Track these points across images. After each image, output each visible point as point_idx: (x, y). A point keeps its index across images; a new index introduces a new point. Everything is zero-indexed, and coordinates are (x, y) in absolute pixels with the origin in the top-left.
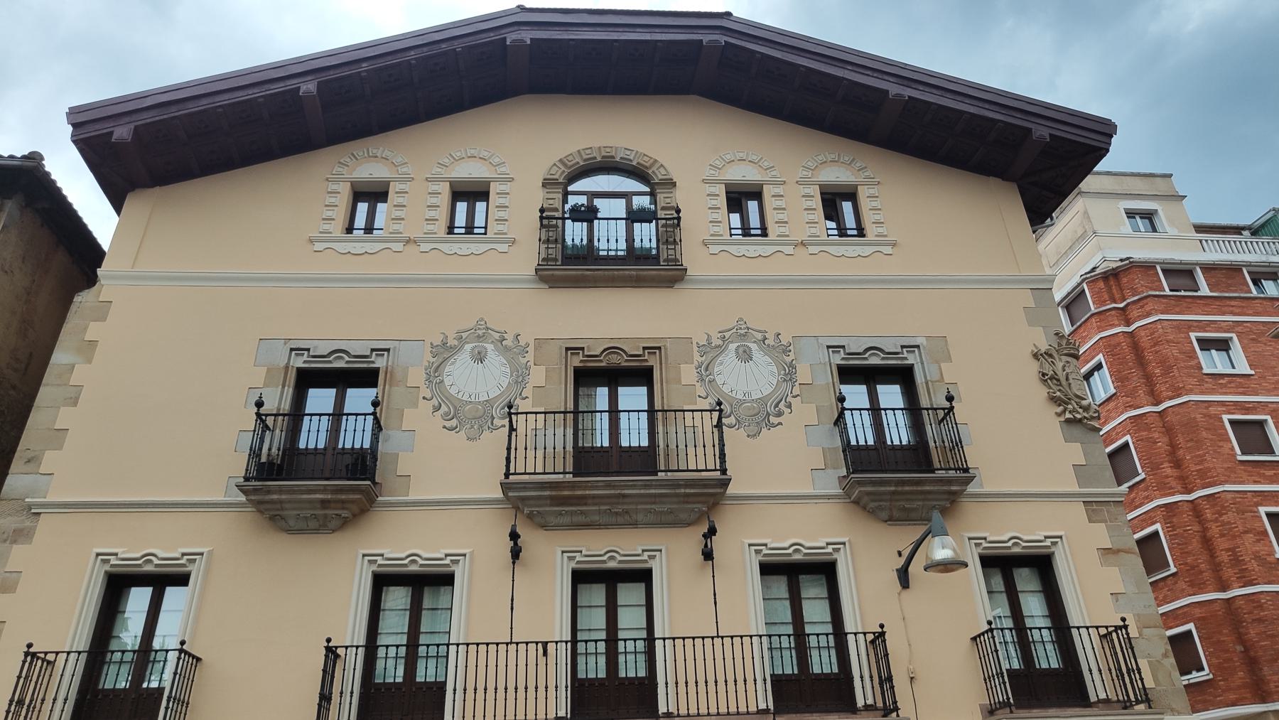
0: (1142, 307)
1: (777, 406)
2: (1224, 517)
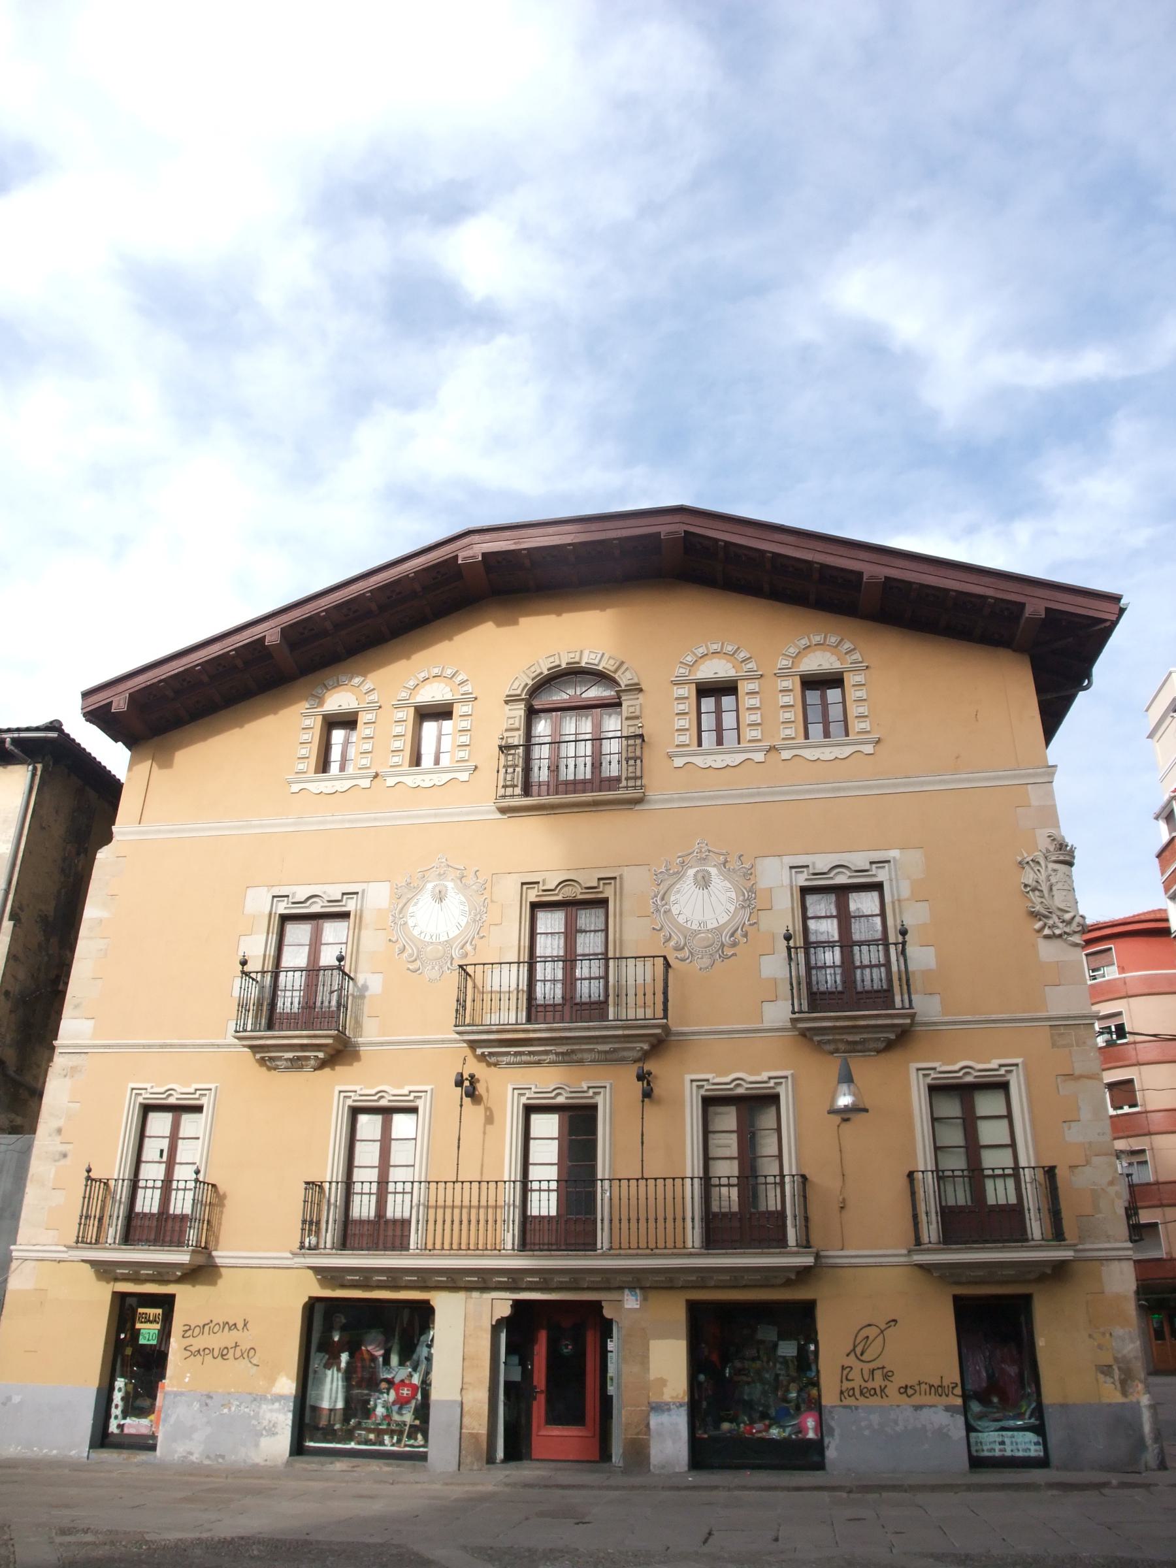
1: (732, 935)
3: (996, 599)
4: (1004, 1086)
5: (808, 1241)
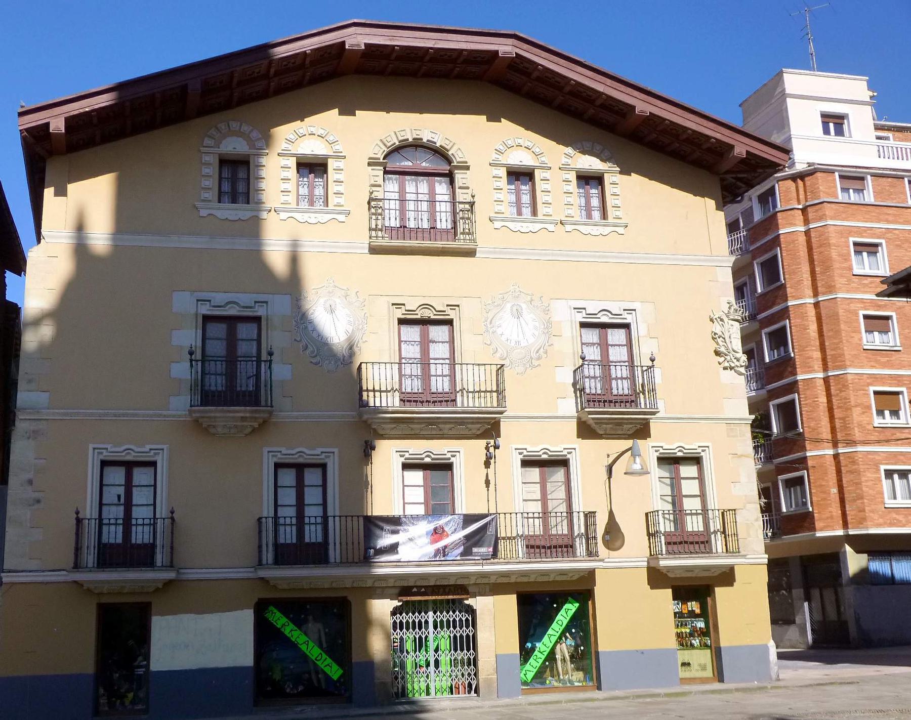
0: (817, 211)
2: (843, 394)
3: (694, 131)
4: (153, 464)
5: (172, 562)
